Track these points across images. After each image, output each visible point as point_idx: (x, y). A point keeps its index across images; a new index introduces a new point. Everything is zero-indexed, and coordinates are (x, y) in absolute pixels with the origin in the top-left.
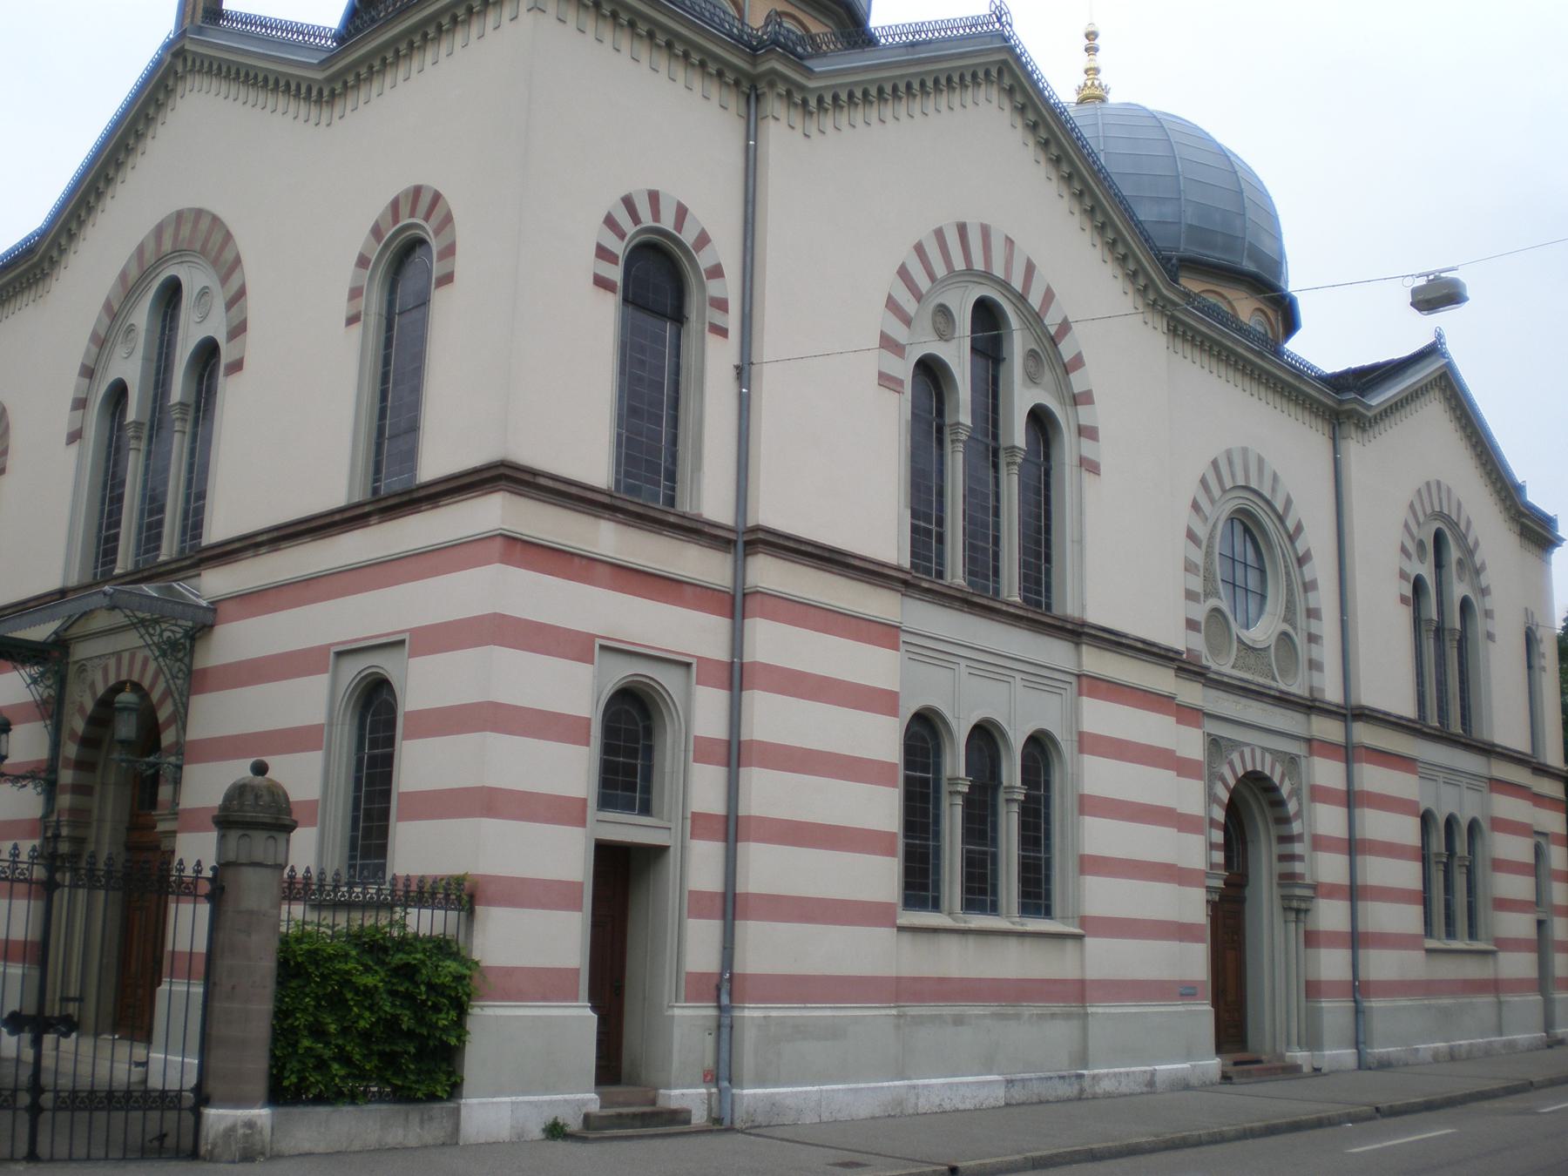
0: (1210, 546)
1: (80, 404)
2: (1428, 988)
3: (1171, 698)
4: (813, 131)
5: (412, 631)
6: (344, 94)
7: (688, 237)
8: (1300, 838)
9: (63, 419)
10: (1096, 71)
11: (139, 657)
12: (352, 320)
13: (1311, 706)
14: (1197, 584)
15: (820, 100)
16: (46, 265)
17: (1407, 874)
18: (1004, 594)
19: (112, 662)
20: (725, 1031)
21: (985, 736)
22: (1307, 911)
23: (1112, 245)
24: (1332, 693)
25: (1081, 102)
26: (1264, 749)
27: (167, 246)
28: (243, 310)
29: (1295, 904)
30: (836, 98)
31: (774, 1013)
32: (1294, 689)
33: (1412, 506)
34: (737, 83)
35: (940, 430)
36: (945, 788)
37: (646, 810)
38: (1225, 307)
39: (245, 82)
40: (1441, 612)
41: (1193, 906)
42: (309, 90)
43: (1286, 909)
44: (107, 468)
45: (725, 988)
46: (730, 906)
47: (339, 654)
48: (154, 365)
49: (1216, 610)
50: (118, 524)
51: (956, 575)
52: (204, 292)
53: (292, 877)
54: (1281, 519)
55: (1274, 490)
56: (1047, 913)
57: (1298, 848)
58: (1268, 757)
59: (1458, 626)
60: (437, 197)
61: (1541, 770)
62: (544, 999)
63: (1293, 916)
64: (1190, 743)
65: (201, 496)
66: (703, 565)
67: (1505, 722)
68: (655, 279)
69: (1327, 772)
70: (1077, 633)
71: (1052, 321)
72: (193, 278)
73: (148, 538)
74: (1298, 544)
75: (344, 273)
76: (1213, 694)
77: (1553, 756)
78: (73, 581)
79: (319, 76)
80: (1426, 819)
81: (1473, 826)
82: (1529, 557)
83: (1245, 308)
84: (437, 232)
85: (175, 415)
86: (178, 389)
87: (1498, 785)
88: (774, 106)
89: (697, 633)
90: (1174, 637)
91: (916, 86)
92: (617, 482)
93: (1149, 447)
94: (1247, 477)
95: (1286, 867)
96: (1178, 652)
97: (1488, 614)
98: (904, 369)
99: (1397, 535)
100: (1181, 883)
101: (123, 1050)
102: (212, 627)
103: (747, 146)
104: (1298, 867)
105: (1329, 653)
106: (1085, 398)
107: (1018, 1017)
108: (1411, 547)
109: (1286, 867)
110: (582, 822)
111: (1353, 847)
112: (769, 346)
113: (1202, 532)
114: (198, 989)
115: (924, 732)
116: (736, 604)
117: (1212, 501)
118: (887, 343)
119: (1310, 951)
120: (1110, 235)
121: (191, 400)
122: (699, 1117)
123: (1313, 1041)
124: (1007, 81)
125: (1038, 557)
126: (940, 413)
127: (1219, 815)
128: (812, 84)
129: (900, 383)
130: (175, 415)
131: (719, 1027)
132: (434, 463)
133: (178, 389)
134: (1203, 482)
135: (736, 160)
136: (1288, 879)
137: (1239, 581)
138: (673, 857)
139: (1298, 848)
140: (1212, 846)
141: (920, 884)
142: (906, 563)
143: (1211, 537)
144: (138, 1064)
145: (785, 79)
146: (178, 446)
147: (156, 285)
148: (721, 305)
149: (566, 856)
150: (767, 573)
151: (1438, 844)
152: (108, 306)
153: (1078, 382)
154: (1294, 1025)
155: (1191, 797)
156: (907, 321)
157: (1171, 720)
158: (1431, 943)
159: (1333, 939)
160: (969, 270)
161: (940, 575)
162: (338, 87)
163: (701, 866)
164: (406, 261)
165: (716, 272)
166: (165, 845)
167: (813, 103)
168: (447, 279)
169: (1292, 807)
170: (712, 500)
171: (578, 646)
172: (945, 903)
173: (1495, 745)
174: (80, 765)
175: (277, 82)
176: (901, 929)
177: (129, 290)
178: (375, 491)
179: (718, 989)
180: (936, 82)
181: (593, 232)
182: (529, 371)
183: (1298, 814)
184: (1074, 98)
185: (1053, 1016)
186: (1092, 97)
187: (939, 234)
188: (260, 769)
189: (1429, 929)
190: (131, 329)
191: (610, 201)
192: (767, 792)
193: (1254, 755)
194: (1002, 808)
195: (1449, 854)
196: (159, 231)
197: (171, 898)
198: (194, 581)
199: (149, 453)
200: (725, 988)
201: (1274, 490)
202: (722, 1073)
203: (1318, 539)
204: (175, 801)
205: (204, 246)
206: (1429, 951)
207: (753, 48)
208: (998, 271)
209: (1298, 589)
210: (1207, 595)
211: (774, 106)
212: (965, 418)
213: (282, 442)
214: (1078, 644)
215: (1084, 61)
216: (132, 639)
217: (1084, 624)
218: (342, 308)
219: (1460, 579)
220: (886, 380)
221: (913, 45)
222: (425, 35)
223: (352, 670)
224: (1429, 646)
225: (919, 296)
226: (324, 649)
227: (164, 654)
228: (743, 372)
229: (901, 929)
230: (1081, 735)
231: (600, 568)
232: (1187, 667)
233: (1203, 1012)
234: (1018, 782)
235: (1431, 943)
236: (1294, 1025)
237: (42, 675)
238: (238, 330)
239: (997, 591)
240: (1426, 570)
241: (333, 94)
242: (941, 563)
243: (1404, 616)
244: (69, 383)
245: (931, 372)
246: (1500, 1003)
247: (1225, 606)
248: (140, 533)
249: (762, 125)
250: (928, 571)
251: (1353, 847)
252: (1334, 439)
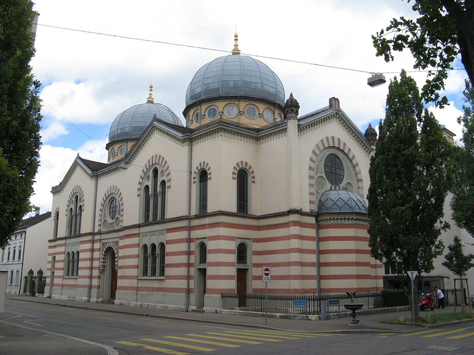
1: (67, 210)
7: (248, 168)
21: (154, 246)
47: (196, 239)
86: (159, 189)
129: (313, 185)
133: (159, 189)
138: (250, 270)
147: (152, 169)
215: (234, 42)
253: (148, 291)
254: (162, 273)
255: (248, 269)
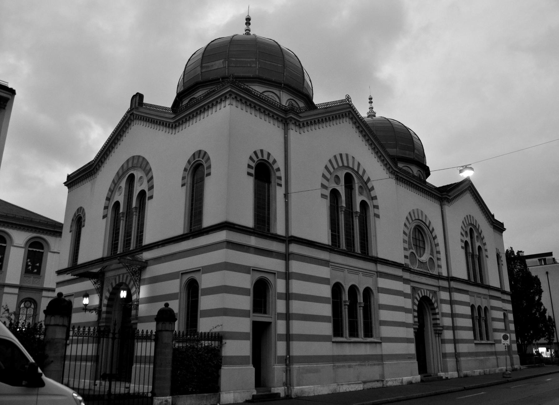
0: (410, 236)
1: (106, 208)
2: (476, 354)
3: (402, 277)
4: (302, 132)
5: (202, 267)
6: (179, 126)
7: (271, 161)
8: (438, 314)
9: (101, 212)
10: (372, 108)
11: (125, 276)
12: (183, 185)
13: (439, 277)
14: (407, 246)
15: (303, 124)
16: (95, 170)
17: (468, 323)
18: (356, 251)
19: (117, 277)
20: (288, 371)
21: (353, 289)
22: (441, 334)
23: (380, 157)
24: (445, 274)
25: (368, 117)
26: (427, 290)
27: (130, 165)
28: (153, 182)
29: (437, 332)
30: (307, 123)
31: (301, 366)
32: (434, 273)
33: (463, 222)
34: (282, 121)
35: (338, 208)
36: (343, 304)
37: (265, 312)
38: (411, 172)
39: (151, 122)
40: (473, 250)
41: (410, 333)
42: (169, 125)
43: (435, 333)
44: (114, 225)
45: (288, 360)
46: (288, 338)
47: (182, 274)
48: (127, 197)
49: (412, 253)
50: (118, 240)
51: (343, 246)
52: (141, 178)
53: (175, 334)
54: (428, 228)
55: (426, 220)
56: (372, 336)
57: (438, 316)
58: (428, 292)
59: (477, 254)
60: (205, 153)
61: (504, 292)
62: (241, 364)
63: (437, 335)
64: (407, 289)
65: (142, 232)
66: (279, 247)
67: (493, 280)
68: (263, 172)
69: (444, 295)
70: (377, 260)
71: (365, 179)
72: (138, 174)
73: (127, 244)
74: (433, 234)
75: (180, 173)
76: (413, 275)
77: (507, 288)
78: (105, 255)
79: (172, 121)
80: (472, 307)
81: (486, 308)
82: (497, 234)
83: (415, 170)
84: (206, 162)
85: (134, 210)
87: (492, 297)
88: (292, 126)
89: (277, 265)
90: (402, 261)
91: (328, 119)
92: (255, 226)
93: (392, 206)
94: (418, 217)
95: (435, 322)
96: (403, 265)
97: (486, 250)
98: (327, 193)
99: (459, 230)
100: (407, 327)
101: (123, 384)
102: (146, 267)
103: (285, 137)
104: (438, 322)
105: (443, 263)
106: (375, 198)
107: (365, 365)
108: (464, 233)
109: (435, 322)
110: (249, 317)
111: (453, 315)
112: (293, 188)
113: (407, 232)
114: (152, 366)
115: (337, 289)
116: (287, 257)
117: (410, 223)
118: (323, 186)
119: (443, 345)
120: (379, 154)
121: (138, 206)
122: (282, 395)
123: (445, 370)
124: (351, 116)
125: (364, 241)
126: (337, 204)
127: (416, 308)
128: (301, 120)
129: (327, 196)
130: (134, 210)
131: (287, 370)
132: (207, 222)
134: (407, 218)
135: (282, 140)
136: (436, 325)
137: (418, 245)
138: (273, 325)
139: (438, 316)
140: (414, 317)
141: (338, 331)
142: (330, 244)
143: (410, 233)
144: (127, 388)
145: (294, 119)
146: (135, 219)
147: (127, 176)
148: (280, 178)
149: (244, 325)
150: (294, 248)
151: (476, 314)
152: (113, 181)
153: (373, 194)
154: (440, 365)
155: (408, 303)
156: (328, 180)
157: (402, 283)
158: (476, 342)
159: (449, 341)
160: (343, 166)
161: (339, 247)
162: (177, 124)
163: (280, 327)
164: (197, 170)
165: (278, 170)
166: (134, 326)
167: (301, 125)
168: (209, 174)
169: (435, 305)
170: (280, 229)
171: (246, 269)
172: (344, 335)
173: (490, 286)
174: (108, 306)
175: (160, 122)
176: (333, 342)
177: (119, 177)
178: (191, 230)
179: (286, 360)
180: (333, 117)
181: (246, 161)
182: (229, 198)
183: (437, 307)
184: (366, 116)
185: (375, 365)
186: (372, 114)
187: (335, 157)
188: (167, 305)
189: (475, 338)
190: (120, 187)
191: (251, 153)
192: (297, 307)
193: (425, 291)
194: (358, 309)
195: (480, 317)
196: (128, 161)
197: (136, 341)
198: (141, 255)
199: (126, 221)
200: (288, 360)
201: (426, 220)
202: (288, 384)
203: (438, 232)
204: (137, 315)
205: (141, 165)
206: (476, 344)
207: (285, 111)
208: (351, 166)
209: (434, 246)
210: (409, 249)
211: (292, 126)
212: (344, 205)
213: (164, 217)
214: (376, 264)
216: (124, 271)
217: (378, 258)
218: (180, 182)
219: (478, 241)
220: (323, 196)
221: (326, 108)
222: (201, 111)
223: (186, 278)
224: (470, 260)
225: (331, 173)
226: (178, 272)
227: (133, 275)
228: (286, 195)
229: (333, 342)
230: (378, 288)
231: (251, 249)
232: (404, 268)
233: (415, 364)
234: (362, 301)
235: (476, 342)
236: (440, 365)
237: (97, 281)
238: (151, 188)
239: (354, 250)
240: (468, 239)
241: (176, 125)
242: (339, 243)
243: (463, 252)
244: (103, 202)
245: (335, 193)
246: (497, 358)
247: (414, 251)
248: (124, 242)
249: (289, 131)
250: (336, 246)
251: (453, 315)
252: (441, 205)
253: (483, 356)
254: (368, 332)
255: (269, 324)
